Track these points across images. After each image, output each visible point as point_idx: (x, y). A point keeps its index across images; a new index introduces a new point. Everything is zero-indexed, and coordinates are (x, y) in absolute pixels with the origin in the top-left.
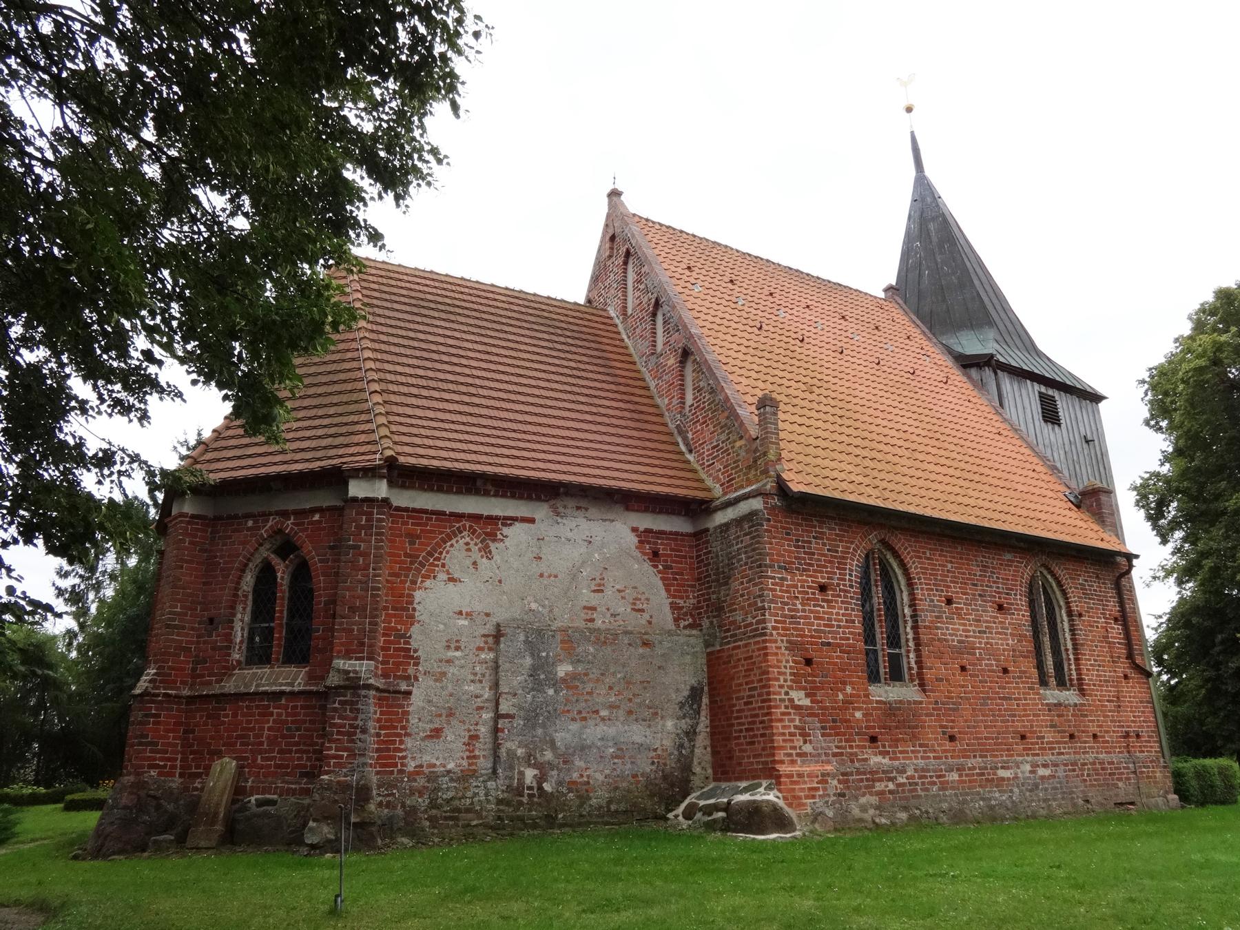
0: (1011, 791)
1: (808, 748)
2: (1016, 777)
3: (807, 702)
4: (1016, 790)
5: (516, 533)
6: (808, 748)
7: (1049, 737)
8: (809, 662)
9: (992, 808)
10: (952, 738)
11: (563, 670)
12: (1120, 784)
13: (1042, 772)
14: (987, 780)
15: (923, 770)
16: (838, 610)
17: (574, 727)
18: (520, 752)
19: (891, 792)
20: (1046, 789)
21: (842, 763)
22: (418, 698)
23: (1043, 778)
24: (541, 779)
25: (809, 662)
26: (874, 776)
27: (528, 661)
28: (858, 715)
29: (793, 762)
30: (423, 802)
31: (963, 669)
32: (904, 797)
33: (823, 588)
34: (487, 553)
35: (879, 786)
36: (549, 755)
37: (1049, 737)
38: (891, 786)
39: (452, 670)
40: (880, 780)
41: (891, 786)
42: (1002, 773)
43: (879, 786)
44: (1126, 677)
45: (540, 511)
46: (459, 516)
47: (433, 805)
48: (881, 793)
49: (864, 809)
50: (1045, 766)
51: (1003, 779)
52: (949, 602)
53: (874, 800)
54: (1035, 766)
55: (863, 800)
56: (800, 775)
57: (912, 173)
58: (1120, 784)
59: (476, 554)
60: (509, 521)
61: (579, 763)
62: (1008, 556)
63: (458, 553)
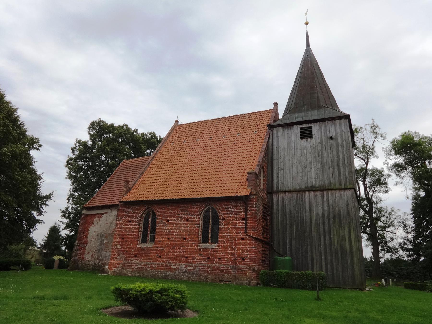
0: (175, 272)
1: (118, 257)
2: (178, 269)
3: (120, 247)
4: (177, 272)
5: (104, 216)
6: (118, 257)
7: (197, 258)
8: (123, 238)
9: (167, 276)
10: (160, 257)
11: (105, 241)
12: (225, 275)
13: (189, 268)
14: (167, 268)
15: (146, 264)
16: (133, 226)
17: (105, 252)
18: (97, 257)
19: (136, 269)
20: (189, 273)
21: (126, 261)
22: (87, 248)
23: (189, 270)
24: (99, 262)
25: (123, 238)
26: (132, 264)
27: (100, 240)
28: (133, 250)
29: (114, 260)
30: (84, 265)
31: (169, 239)
32: (139, 270)
33: (130, 222)
34: (100, 220)
35: (132, 267)
36: (101, 258)
37: (197, 258)
38: (136, 267)
39: (92, 242)
40: (133, 266)
41: (136, 267)
42: (173, 267)
43: (132, 267)
44: (243, 239)
45: (108, 211)
46: (96, 214)
47: (85, 266)
48: (133, 268)
49: (127, 272)
50: (190, 266)
51: (173, 269)
52: (168, 221)
53: (131, 270)
54: (187, 266)
55: (128, 270)
56: (113, 263)
57: (304, 47)
58: (225, 275)
59: (98, 221)
60: (103, 214)
61: (104, 259)
62: (194, 205)
63: (96, 221)
